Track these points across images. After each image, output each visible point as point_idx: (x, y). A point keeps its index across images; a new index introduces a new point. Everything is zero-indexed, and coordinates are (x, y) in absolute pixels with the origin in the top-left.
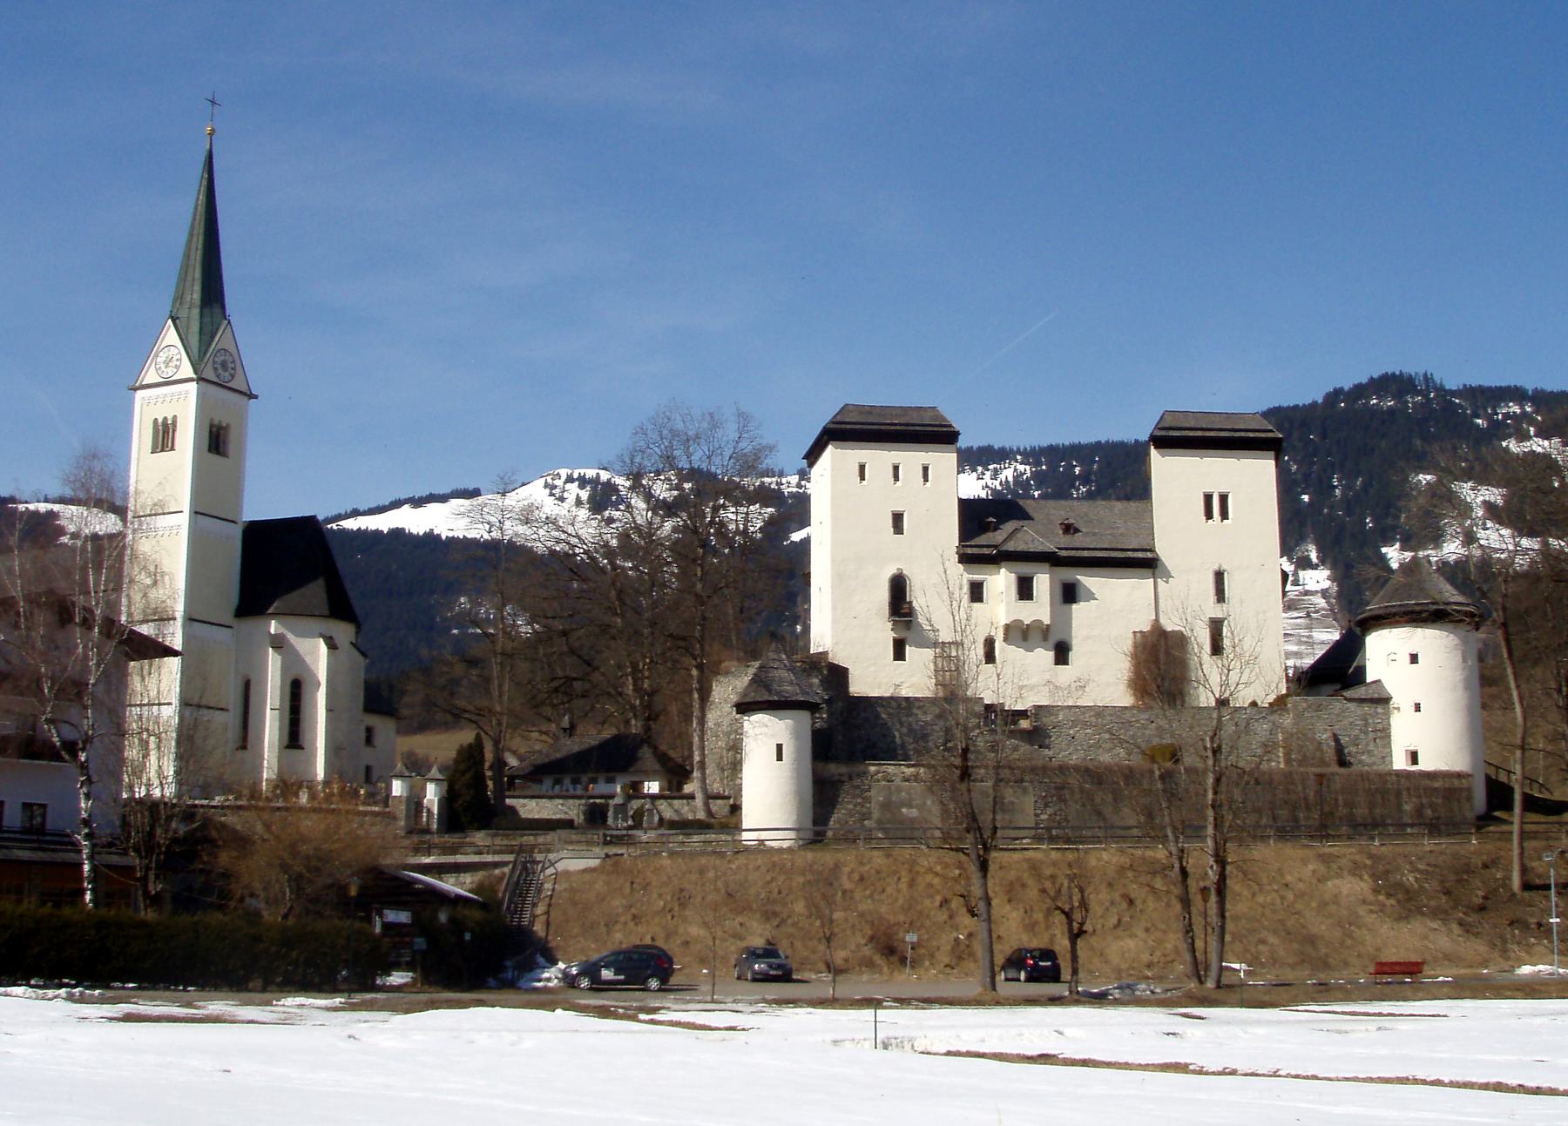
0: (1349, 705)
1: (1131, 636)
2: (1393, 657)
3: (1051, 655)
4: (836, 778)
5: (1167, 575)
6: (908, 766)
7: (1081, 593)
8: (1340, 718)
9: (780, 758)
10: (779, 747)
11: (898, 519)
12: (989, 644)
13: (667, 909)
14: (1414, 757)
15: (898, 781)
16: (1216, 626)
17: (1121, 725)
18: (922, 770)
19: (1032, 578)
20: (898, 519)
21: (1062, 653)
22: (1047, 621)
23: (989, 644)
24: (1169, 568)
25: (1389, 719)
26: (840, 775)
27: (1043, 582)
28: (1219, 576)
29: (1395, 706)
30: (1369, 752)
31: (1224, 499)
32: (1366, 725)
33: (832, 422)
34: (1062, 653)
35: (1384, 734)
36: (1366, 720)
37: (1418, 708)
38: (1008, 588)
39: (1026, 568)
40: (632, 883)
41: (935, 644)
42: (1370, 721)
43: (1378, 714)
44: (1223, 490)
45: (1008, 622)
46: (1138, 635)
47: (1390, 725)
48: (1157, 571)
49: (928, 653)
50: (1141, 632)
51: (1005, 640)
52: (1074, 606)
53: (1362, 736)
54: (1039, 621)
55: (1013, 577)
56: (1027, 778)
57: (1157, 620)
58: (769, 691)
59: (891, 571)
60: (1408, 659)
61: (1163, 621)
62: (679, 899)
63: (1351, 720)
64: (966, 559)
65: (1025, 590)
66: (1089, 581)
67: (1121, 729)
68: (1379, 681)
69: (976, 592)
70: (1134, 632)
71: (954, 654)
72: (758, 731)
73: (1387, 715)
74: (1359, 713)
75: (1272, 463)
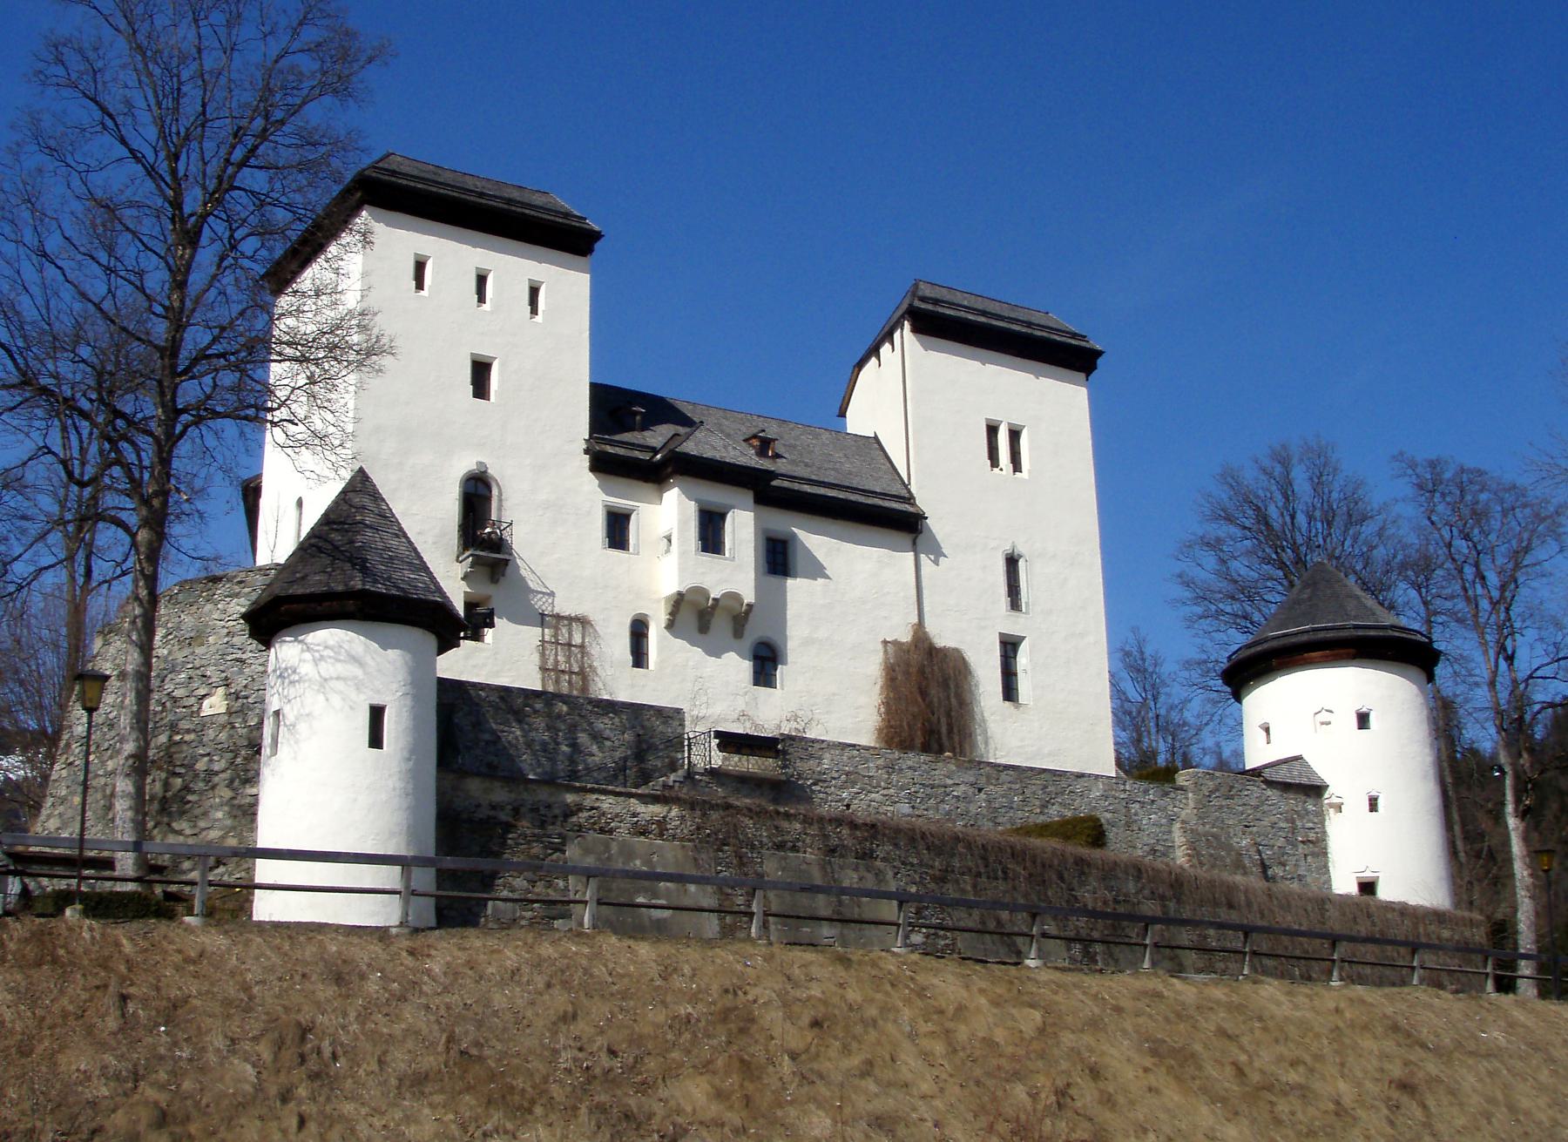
0: (1269, 792)
1: (880, 647)
2: (1324, 716)
3: (745, 667)
4: (484, 813)
5: (937, 552)
6: (645, 798)
7: (799, 562)
8: (1259, 815)
9: (376, 740)
10: (377, 713)
11: (480, 372)
12: (639, 631)
13: (273, 1090)
14: (1368, 887)
15: (623, 832)
16: (1009, 646)
17: (929, 790)
18: (675, 811)
19: (723, 516)
20: (480, 372)
21: (766, 663)
22: (749, 596)
23: (639, 631)
24: (939, 537)
25: (1323, 822)
26: (493, 807)
27: (742, 526)
28: (1012, 562)
29: (1334, 800)
30: (1300, 878)
31: (1015, 435)
32: (1294, 830)
33: (373, 167)
34: (766, 663)
35: (1318, 847)
36: (1293, 821)
37: (1373, 805)
38: (683, 524)
39: (716, 494)
40: (124, 998)
41: (542, 619)
42: (1299, 824)
43: (1308, 812)
44: (1017, 421)
45: (683, 589)
46: (890, 648)
47: (1325, 832)
48: (921, 539)
49: (532, 635)
50: (895, 643)
51: (670, 626)
52: (790, 582)
53: (1289, 849)
54: (735, 597)
55: (692, 508)
56: (880, 853)
57: (921, 623)
58: (365, 570)
59: (465, 464)
60: (1354, 721)
61: (931, 627)
62: (303, 1059)
63: (1273, 819)
64: (603, 464)
65: (711, 535)
66: (815, 541)
67: (929, 797)
68: (1298, 758)
69: (617, 530)
70: (885, 642)
71: (577, 639)
72: (327, 669)
73: (1321, 816)
74: (1284, 808)
75: (1084, 391)
